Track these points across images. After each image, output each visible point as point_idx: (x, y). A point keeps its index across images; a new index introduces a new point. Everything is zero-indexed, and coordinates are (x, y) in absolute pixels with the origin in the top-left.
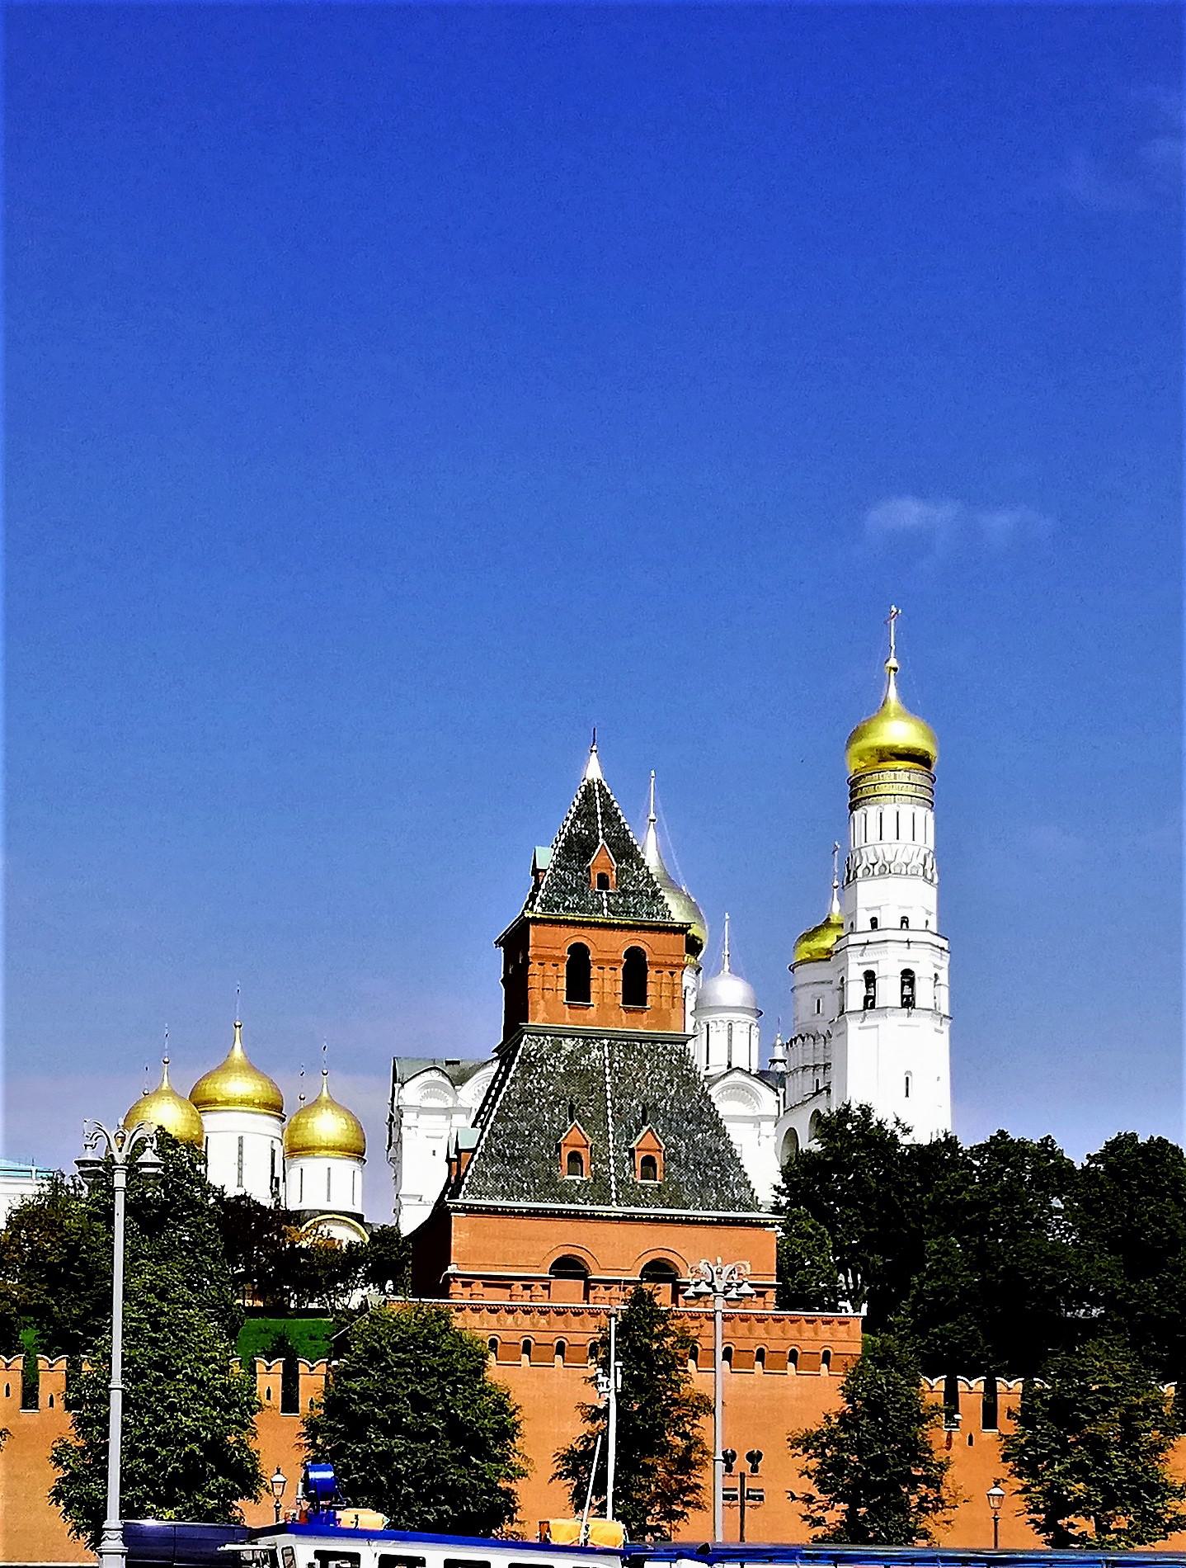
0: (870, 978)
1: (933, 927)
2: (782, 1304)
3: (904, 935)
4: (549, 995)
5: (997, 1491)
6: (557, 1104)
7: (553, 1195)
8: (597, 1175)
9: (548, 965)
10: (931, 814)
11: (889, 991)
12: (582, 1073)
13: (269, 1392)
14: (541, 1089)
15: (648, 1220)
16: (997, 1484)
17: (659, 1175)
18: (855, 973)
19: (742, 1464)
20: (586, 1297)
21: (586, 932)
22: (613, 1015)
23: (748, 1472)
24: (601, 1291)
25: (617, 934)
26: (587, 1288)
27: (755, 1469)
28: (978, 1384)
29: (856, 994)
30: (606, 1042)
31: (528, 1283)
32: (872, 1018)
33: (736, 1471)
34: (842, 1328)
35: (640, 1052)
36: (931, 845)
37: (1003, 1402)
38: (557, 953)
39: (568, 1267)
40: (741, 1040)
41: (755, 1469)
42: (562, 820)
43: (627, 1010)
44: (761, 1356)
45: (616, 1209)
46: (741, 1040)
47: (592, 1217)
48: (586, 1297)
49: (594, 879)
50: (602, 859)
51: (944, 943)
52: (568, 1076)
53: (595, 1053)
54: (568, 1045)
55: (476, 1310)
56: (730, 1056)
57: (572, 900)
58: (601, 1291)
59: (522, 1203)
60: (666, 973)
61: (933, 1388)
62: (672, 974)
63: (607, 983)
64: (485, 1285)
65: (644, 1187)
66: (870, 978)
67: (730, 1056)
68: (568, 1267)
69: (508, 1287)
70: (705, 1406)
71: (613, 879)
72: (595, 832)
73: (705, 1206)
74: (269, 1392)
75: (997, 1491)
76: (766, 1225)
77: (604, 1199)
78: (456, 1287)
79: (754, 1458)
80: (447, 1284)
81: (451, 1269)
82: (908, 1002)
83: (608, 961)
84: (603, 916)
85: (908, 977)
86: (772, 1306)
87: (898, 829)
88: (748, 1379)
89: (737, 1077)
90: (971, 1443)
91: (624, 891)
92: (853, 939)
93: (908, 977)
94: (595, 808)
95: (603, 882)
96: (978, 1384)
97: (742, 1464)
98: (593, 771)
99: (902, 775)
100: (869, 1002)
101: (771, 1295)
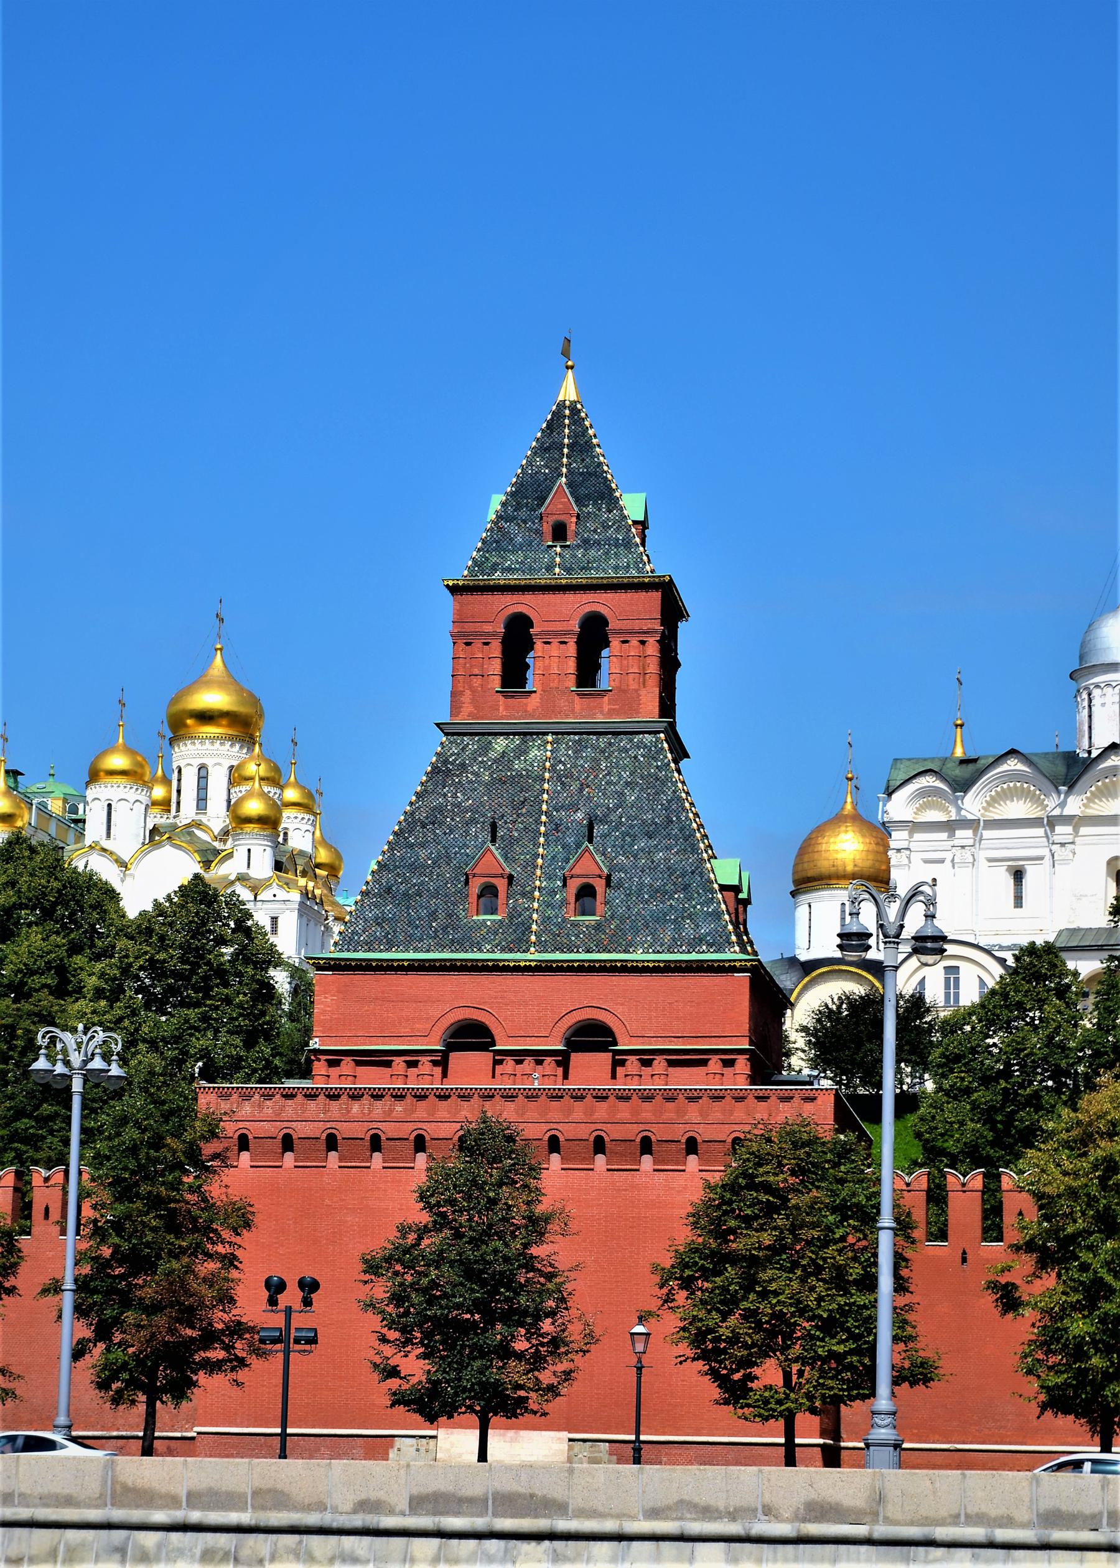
4: (477, 682)
5: (639, 1329)
6: (473, 821)
9: (477, 644)
13: (47, 1209)
14: (459, 805)
15: (527, 969)
16: (641, 1320)
17: (600, 908)
19: (291, 1297)
20: (614, 1076)
21: (528, 598)
22: (562, 703)
23: (297, 1305)
24: (509, 1064)
25: (570, 597)
26: (617, 1063)
27: (307, 1302)
30: (550, 738)
31: (412, 1059)
33: (282, 1305)
34: (670, 1105)
38: (488, 628)
39: (471, 1035)
41: (307, 1302)
42: (514, 454)
43: (581, 695)
45: (533, 956)
48: (614, 1076)
49: (547, 528)
50: (560, 501)
53: (534, 753)
55: (399, 1096)
58: (509, 1064)
60: (634, 642)
62: (643, 643)
64: (358, 1063)
65: (575, 925)
68: (471, 1035)
69: (388, 1064)
70: (242, 1219)
71: (572, 527)
72: (566, 474)
74: (47, 1209)
75: (639, 1329)
76: (734, 970)
77: (521, 943)
78: (320, 1067)
79: (309, 1287)
80: (309, 1062)
81: (315, 1044)
83: (556, 634)
86: (742, 1079)
88: (679, 1180)
90: (964, 1260)
91: (586, 541)
94: (566, 438)
97: (291, 1297)
98: (568, 391)
101: (743, 1065)
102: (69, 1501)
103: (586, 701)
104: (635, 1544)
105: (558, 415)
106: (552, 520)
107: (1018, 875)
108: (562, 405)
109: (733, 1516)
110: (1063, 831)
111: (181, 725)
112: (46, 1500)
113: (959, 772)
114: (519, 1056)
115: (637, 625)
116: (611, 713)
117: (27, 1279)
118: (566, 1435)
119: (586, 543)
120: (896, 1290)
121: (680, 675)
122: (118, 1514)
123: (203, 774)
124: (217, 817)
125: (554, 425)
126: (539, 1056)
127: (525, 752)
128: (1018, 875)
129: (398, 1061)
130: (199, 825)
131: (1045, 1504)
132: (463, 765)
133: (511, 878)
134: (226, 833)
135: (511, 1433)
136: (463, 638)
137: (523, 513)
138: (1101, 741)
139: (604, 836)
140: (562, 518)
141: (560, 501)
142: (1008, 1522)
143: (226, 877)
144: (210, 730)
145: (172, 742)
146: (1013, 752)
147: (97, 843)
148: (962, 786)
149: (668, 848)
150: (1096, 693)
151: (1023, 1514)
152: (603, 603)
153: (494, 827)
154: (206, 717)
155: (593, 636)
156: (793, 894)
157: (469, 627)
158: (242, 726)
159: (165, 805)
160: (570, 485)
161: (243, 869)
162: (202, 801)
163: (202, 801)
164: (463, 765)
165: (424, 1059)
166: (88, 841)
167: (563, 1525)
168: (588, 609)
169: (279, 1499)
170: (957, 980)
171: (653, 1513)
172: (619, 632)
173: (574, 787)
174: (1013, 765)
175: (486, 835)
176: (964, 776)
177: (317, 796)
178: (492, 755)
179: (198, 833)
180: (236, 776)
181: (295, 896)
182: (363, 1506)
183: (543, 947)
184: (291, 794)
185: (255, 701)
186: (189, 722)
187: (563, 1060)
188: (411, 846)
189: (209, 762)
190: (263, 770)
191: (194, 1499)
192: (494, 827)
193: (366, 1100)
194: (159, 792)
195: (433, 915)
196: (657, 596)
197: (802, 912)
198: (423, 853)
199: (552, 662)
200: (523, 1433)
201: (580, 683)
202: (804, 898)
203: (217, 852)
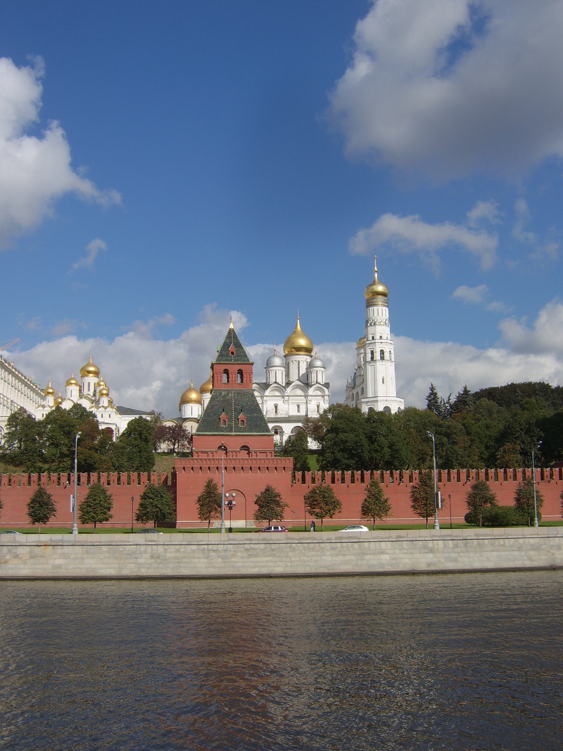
0: (372, 353)
1: (389, 339)
3: (381, 341)
8: (229, 425)
10: (387, 309)
11: (377, 356)
18: (369, 351)
21: (227, 365)
29: (369, 358)
32: (384, 362)
36: (388, 316)
37: (471, 475)
45: (234, 433)
46: (320, 375)
50: (232, 348)
51: (392, 342)
54: (223, 393)
57: (224, 358)
59: (255, 433)
66: (372, 353)
71: (235, 353)
82: (382, 358)
84: (233, 362)
85: (382, 352)
87: (380, 312)
92: (367, 342)
93: (382, 352)
95: (232, 353)
98: (232, 326)
99: (380, 299)
100: (372, 358)
102: (42, 542)
107: (298, 406)
108: (231, 329)
112: (276, 540)
117: (2, 484)
119: (238, 356)
120: (528, 521)
122: (289, 541)
123: (89, 384)
128: (298, 406)
130: (89, 394)
131: (432, 534)
141: (232, 348)
144: (91, 375)
158: (97, 374)
162: (89, 390)
167: (360, 541)
169: (315, 539)
183: (235, 432)
191: (300, 539)
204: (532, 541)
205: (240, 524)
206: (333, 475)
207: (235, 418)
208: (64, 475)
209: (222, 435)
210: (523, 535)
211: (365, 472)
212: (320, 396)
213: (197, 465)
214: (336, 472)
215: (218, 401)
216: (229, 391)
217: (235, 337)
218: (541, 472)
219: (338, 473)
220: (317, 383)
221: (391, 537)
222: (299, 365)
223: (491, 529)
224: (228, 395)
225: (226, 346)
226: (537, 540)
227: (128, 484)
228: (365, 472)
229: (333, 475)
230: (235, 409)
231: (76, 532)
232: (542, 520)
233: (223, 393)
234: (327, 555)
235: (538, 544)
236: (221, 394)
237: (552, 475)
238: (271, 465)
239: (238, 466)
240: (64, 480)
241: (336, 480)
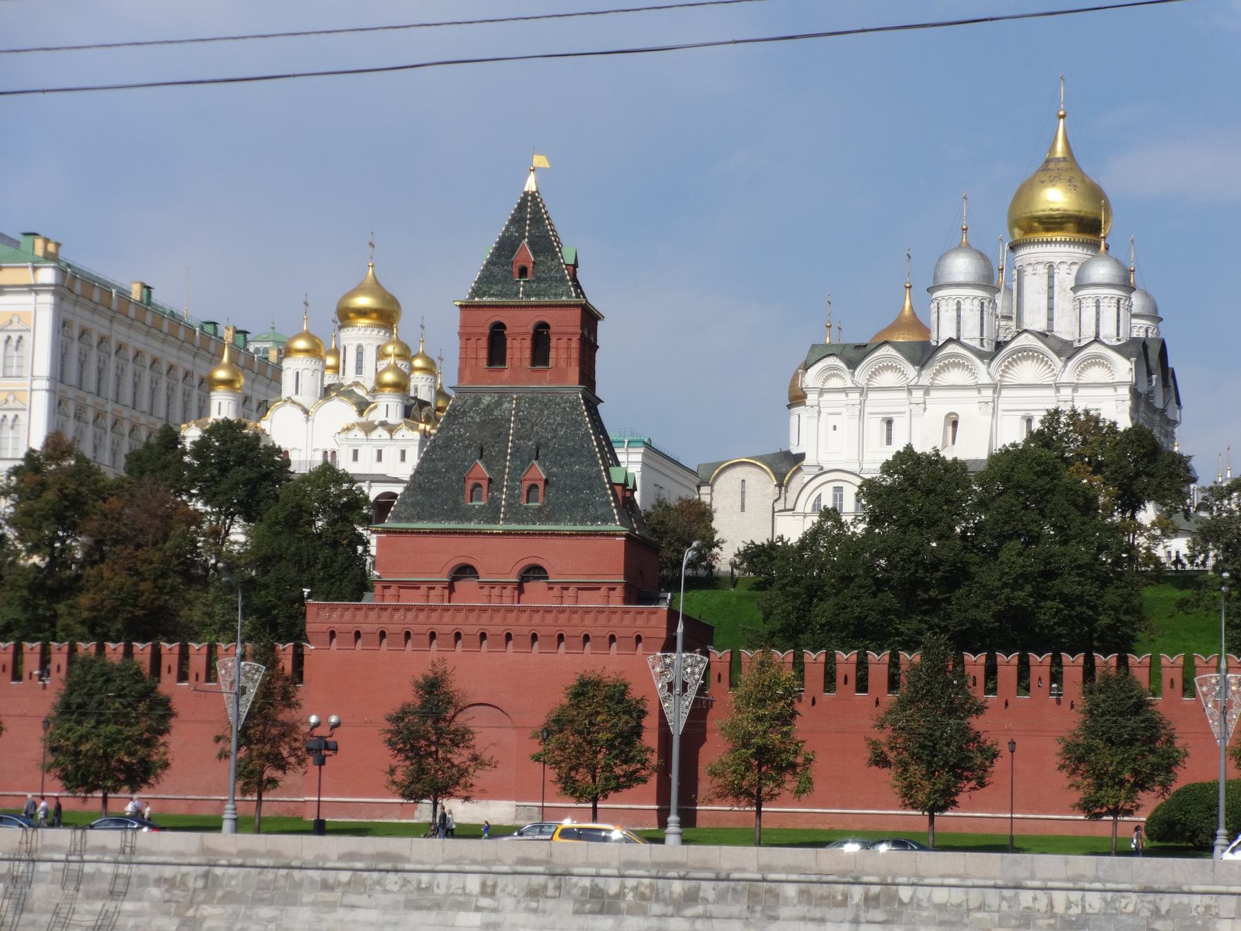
2: (627, 600)
6: (470, 446)
7: (455, 519)
9: (473, 340)
12: (495, 421)
14: (461, 436)
28: (1014, 658)
35: (541, 402)
37: (841, 671)
40: (1109, 314)
44: (586, 638)
45: (501, 527)
47: (479, 533)
49: (516, 271)
50: (525, 253)
52: (483, 423)
53: (506, 405)
56: (1098, 326)
57: (496, 288)
60: (565, 339)
61: (975, 662)
63: (519, 349)
65: (526, 508)
67: (1098, 326)
71: (530, 270)
73: (574, 521)
76: (615, 535)
77: (494, 519)
83: (519, 334)
84: (521, 299)
89: (1096, 349)
96: (1014, 658)
98: (531, 185)
101: (619, 592)
102: (183, 854)
103: (536, 374)
104: (469, 876)
105: (524, 200)
106: (518, 265)
108: (526, 194)
109: (483, 863)
110: (918, 395)
111: (346, 316)
113: (853, 354)
114: (493, 585)
115: (566, 329)
116: (551, 382)
118: (514, 803)
119: (539, 280)
121: (599, 355)
124: (368, 380)
125: (522, 206)
126: (504, 585)
127: (501, 405)
128: (889, 422)
129: (424, 587)
132: (465, 412)
133: (490, 481)
134: (374, 390)
135: (484, 802)
136: (465, 335)
137: (503, 260)
138: (944, 336)
139: (545, 456)
140: (525, 264)
141: (525, 253)
142: (607, 866)
143: (372, 422)
145: (340, 328)
146: (886, 343)
147: (289, 398)
148: (852, 364)
149: (582, 463)
150: (943, 303)
151: (615, 863)
152: (547, 316)
153: (482, 450)
154: (363, 313)
155: (541, 339)
156: (789, 407)
157: (469, 330)
159: (336, 369)
160: (530, 243)
161: (383, 418)
162: (359, 369)
163: (359, 369)
164: (465, 412)
165: (438, 586)
166: (284, 396)
168: (538, 319)
169: (278, 854)
170: (841, 496)
171: (445, 862)
172: (556, 333)
173: (528, 426)
174: (887, 351)
175: (477, 453)
176: (854, 356)
177: (437, 362)
178: (482, 406)
179: (357, 390)
180: (381, 354)
181: (416, 435)
182: (317, 857)
183: (506, 520)
184: (418, 363)
185: (393, 301)
186: (351, 315)
187: (520, 588)
188: (433, 460)
189: (364, 343)
190: (397, 351)
191: (241, 853)
192: (482, 450)
193: (402, 612)
194: (330, 361)
195: (444, 502)
196: (578, 311)
197: (794, 420)
198: (440, 465)
199: (519, 349)
200: (491, 802)
201: (534, 361)
202: (796, 410)
203: (368, 404)
204: (940, 896)
205: (498, 811)
206: (862, 664)
207: (512, 479)
208: (32, 649)
209: (554, 534)
210: (917, 875)
211: (1001, 657)
212: (1049, 386)
213: (370, 625)
214: (872, 656)
215: (467, 426)
216: (503, 395)
217: (539, 218)
218: (826, 664)
219: (846, 659)
220: (957, 341)
221: (500, 861)
222: (1051, 277)
223: (999, 855)
224: (499, 404)
225: (506, 248)
226: (957, 896)
227: (859, 690)
228: (1001, 657)
229: (862, 664)
230: (517, 449)
231: (227, 825)
232: (701, 823)
233: (487, 399)
234: (302, 904)
235: (959, 905)
236: (478, 401)
237: (1056, 677)
238: (599, 629)
239: (470, 628)
240: (31, 662)
241: (840, 680)
